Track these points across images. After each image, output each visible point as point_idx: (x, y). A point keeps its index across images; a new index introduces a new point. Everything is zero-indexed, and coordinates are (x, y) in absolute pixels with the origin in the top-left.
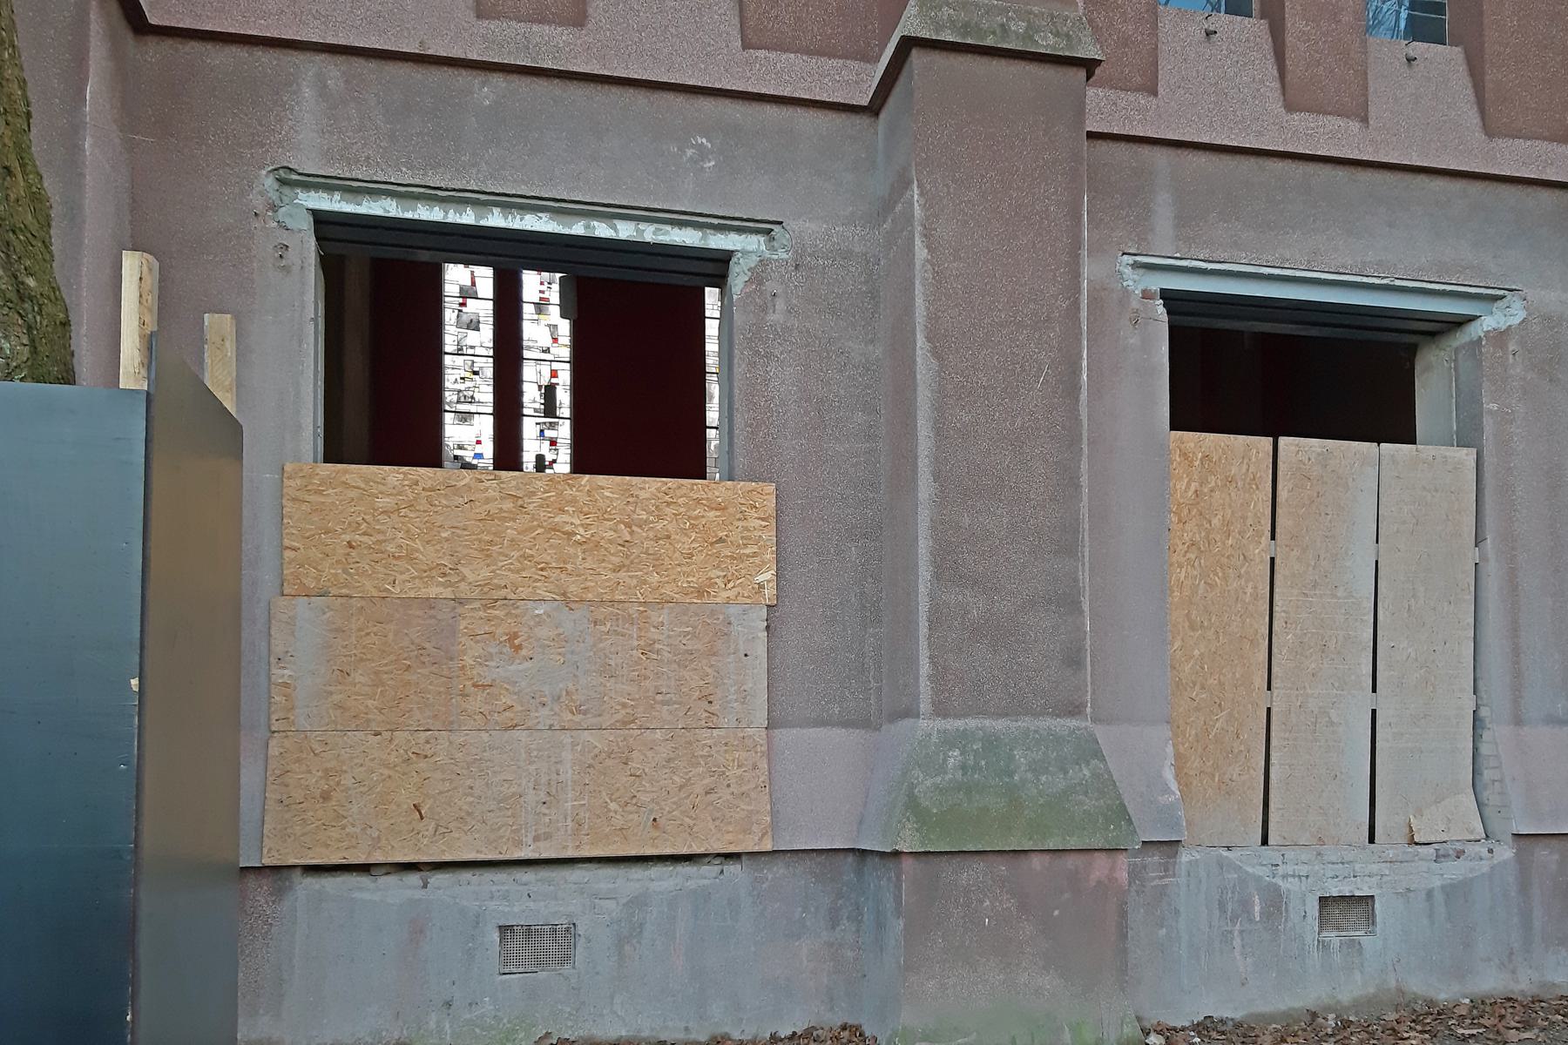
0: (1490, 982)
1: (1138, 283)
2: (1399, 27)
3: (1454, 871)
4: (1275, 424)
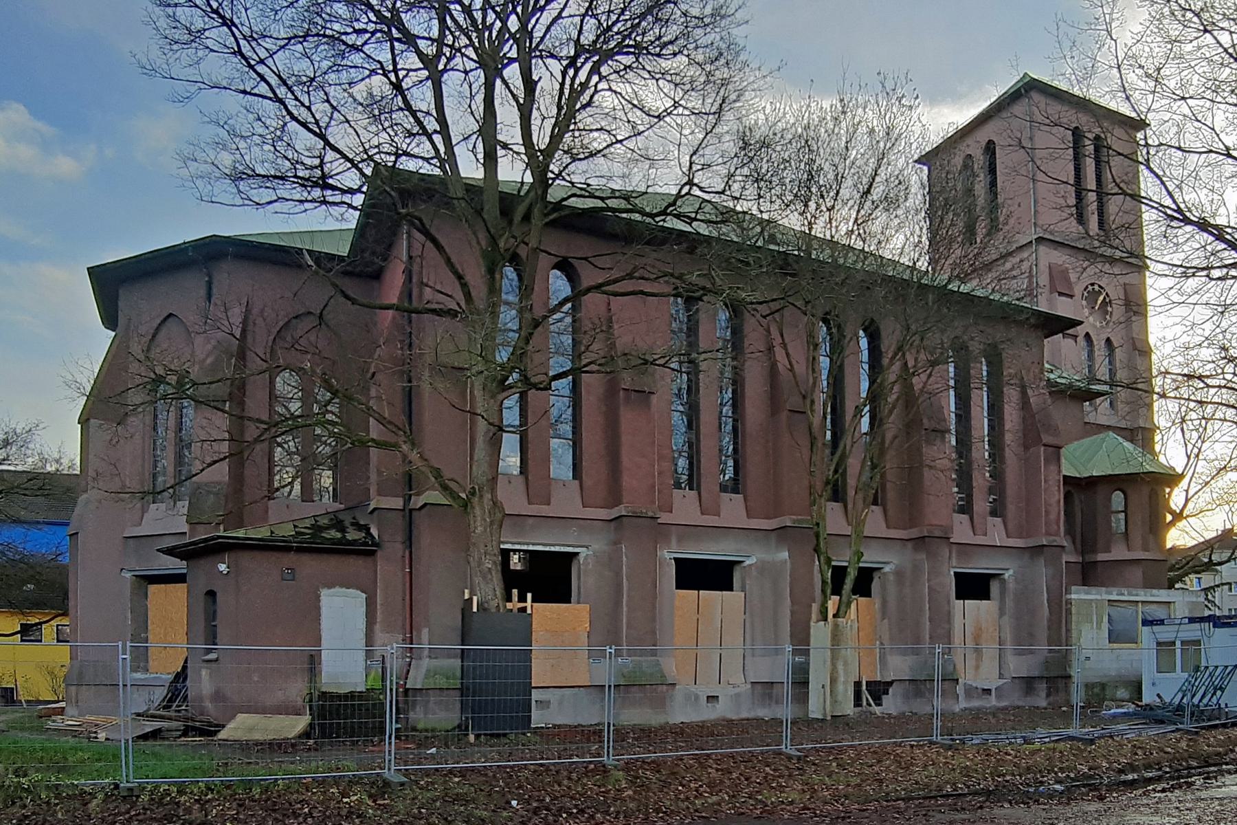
0: (744, 715)
1: (667, 556)
2: (419, 230)
3: (737, 690)
4: (698, 587)
